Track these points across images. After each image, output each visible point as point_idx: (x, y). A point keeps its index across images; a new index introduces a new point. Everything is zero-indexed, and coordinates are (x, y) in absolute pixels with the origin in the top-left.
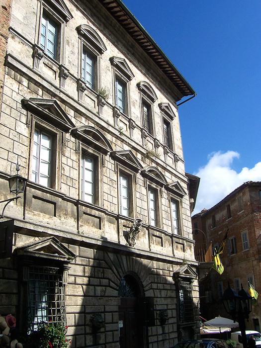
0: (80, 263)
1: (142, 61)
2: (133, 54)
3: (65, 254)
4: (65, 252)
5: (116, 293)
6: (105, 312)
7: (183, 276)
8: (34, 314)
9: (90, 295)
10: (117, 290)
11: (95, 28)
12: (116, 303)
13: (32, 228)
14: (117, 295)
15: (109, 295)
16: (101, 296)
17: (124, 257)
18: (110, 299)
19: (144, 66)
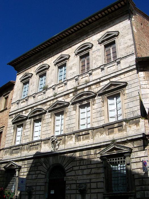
0: (26, 167)
1: (80, 36)
2: (73, 41)
3: (123, 149)
4: (120, 147)
5: (44, 176)
6: (36, 186)
7: (116, 153)
8: (118, 173)
9: (29, 179)
10: (44, 175)
11: (39, 65)
12: (43, 181)
13: (30, 157)
14: (44, 177)
15: (39, 178)
16: (35, 179)
17: (145, 140)
18: (40, 180)
19: (83, 35)
